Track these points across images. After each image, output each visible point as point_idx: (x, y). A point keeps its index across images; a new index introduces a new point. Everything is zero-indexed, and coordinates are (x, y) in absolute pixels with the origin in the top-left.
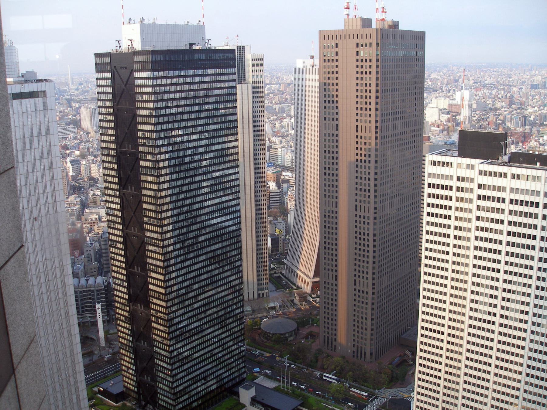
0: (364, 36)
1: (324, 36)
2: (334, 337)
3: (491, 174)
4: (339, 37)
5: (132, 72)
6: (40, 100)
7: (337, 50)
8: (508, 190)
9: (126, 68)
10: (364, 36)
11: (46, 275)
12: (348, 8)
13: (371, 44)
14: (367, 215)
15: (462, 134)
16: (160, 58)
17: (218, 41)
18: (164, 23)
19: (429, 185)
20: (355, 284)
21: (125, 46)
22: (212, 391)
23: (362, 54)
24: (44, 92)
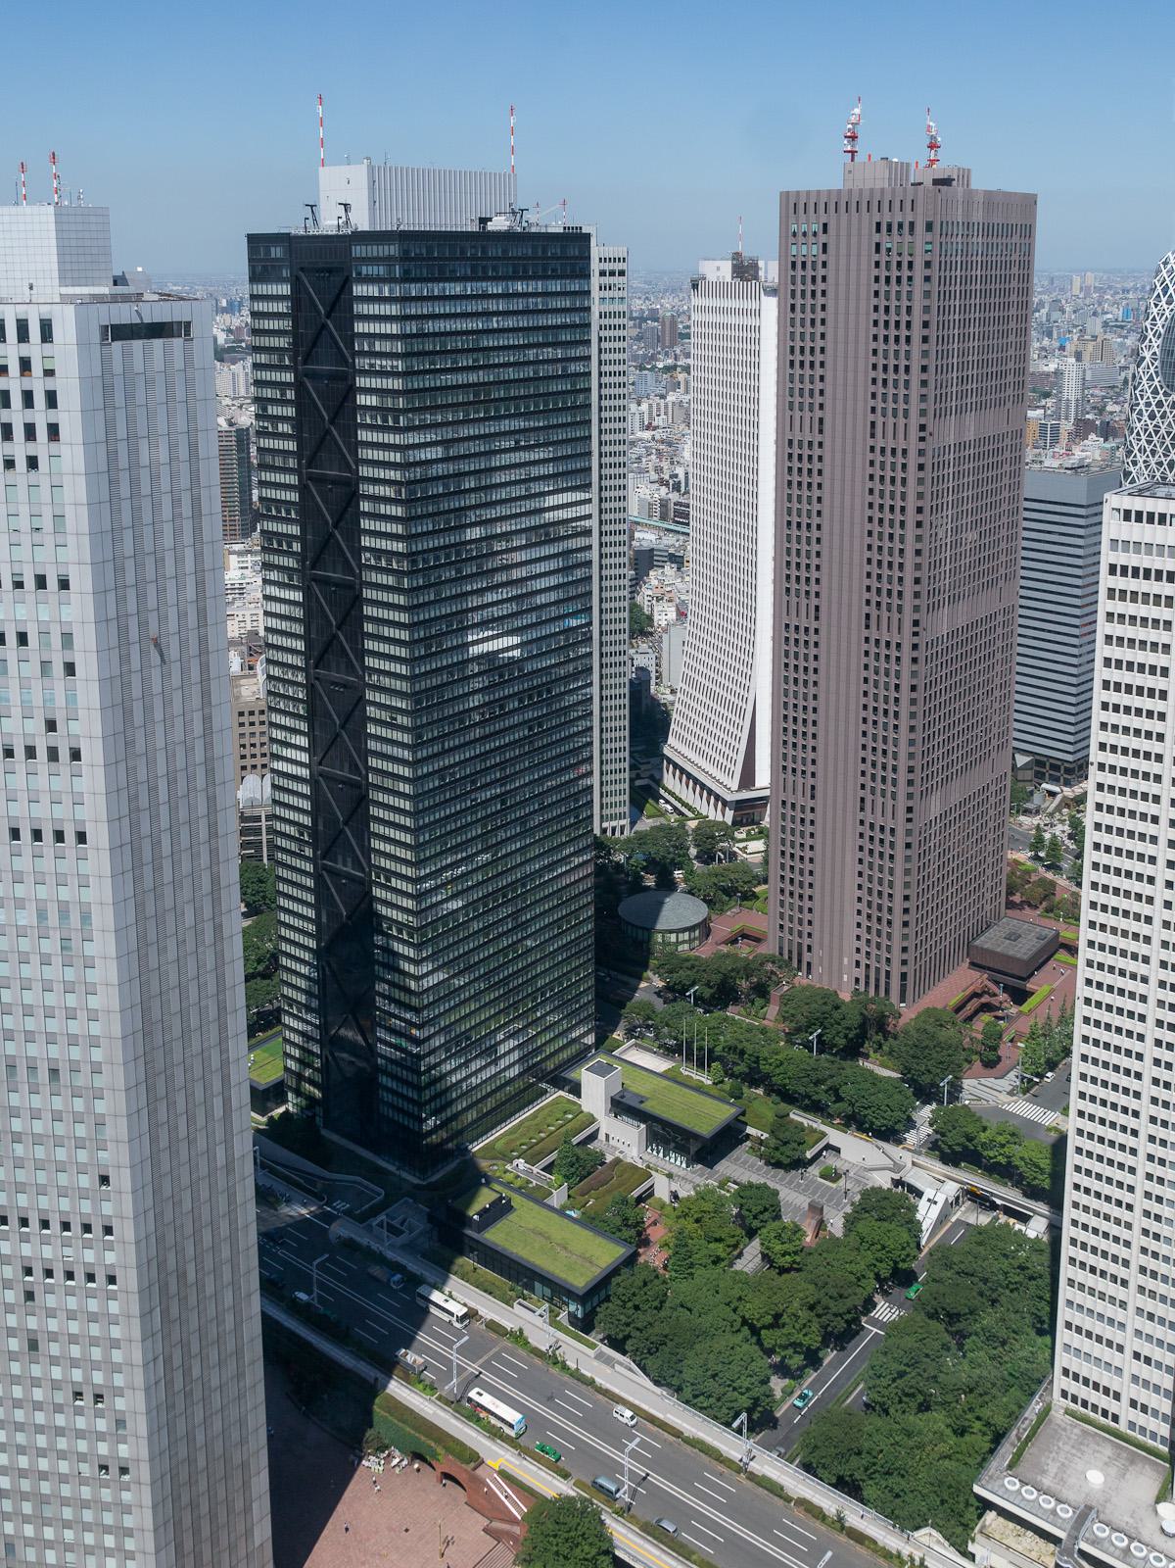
1: (793, 205)
2: (806, 941)
5: (346, 285)
6: (177, 342)
11: (171, 782)
13: (912, 224)
17: (549, 220)
19: (1112, 569)
20: (862, 809)
21: (329, 223)
22: (511, 1081)
24: (188, 324)
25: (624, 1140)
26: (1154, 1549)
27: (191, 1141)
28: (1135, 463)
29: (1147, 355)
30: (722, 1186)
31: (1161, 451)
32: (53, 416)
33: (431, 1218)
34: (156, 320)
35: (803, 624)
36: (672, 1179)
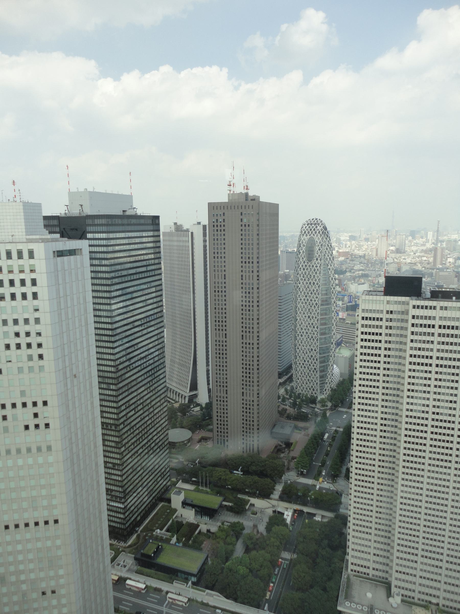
1: (212, 207)
4: (226, 208)
6: (78, 257)
8: (437, 318)
9: (77, 230)
10: (247, 207)
12: (230, 185)
14: (251, 342)
17: (143, 208)
18: (103, 191)
23: (245, 220)
24: (81, 249)
25: (189, 515)
26: (358, 604)
29: (301, 251)
30: (223, 524)
31: (307, 279)
32: (34, 289)
33: (136, 559)
35: (221, 340)
36: (206, 525)
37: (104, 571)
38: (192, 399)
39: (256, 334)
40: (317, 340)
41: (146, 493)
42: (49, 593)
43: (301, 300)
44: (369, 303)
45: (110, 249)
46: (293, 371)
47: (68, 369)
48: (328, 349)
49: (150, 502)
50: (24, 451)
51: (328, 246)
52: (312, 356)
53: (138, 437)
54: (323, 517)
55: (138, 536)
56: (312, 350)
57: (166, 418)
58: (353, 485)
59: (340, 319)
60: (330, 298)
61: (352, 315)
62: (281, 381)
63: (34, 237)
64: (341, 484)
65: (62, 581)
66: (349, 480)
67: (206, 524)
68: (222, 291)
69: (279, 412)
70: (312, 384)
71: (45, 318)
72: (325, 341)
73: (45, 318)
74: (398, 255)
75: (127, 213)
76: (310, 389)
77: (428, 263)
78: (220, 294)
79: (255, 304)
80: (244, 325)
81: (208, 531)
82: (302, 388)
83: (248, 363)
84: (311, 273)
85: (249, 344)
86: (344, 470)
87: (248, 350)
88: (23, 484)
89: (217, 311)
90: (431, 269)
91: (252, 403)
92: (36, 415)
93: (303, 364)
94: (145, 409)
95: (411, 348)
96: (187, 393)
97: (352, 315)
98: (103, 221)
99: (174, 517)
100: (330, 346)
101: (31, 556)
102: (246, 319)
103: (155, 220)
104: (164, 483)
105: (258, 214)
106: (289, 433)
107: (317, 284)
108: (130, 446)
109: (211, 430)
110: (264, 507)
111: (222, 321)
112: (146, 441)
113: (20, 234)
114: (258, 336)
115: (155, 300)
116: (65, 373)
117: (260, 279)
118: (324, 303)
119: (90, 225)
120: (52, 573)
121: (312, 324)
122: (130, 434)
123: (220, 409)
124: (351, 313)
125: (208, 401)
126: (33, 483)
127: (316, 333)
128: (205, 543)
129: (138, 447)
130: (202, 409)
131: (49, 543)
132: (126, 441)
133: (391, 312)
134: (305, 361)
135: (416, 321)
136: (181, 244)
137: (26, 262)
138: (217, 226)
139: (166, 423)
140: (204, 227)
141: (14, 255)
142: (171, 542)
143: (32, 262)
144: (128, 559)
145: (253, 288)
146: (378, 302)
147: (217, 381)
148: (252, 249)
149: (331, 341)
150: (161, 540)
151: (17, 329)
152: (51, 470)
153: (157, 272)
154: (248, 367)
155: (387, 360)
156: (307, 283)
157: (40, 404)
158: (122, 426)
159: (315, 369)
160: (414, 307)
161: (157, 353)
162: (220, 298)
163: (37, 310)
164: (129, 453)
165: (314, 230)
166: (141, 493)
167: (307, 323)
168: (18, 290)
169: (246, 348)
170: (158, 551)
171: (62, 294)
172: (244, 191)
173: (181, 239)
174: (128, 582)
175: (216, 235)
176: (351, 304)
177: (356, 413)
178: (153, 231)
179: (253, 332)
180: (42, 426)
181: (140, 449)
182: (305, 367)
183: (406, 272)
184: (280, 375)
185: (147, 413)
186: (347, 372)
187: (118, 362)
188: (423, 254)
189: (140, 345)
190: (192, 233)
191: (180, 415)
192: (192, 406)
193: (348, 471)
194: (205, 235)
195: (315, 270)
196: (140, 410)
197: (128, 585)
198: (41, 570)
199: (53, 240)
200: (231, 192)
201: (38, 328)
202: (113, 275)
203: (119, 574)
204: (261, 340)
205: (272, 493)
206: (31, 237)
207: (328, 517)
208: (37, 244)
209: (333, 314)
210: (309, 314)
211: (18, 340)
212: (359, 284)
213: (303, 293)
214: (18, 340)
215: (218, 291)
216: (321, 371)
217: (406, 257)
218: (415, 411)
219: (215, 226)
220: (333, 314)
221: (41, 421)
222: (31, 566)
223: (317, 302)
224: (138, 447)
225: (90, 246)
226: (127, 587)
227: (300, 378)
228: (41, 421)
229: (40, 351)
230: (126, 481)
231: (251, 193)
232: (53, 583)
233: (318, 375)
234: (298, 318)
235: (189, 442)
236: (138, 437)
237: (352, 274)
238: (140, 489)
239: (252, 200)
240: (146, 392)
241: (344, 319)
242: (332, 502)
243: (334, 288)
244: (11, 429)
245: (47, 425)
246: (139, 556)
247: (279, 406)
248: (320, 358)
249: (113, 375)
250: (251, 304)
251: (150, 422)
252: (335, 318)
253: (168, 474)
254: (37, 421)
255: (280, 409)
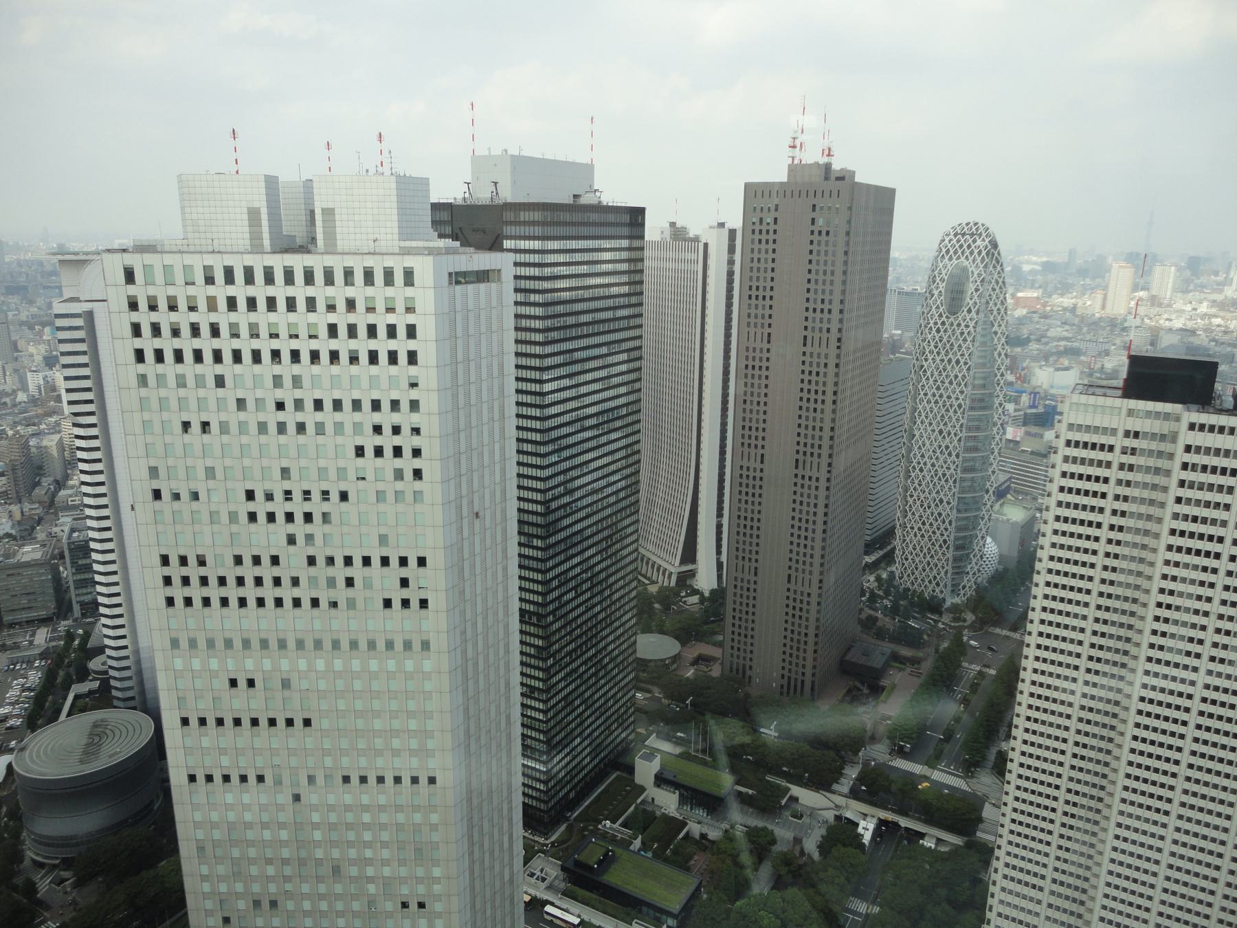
0: (827, 194)
1: (752, 191)
2: (748, 663)
3: (1212, 429)
6: (494, 285)
7: (776, 215)
10: (827, 194)
12: (794, 147)
14: (815, 475)
15: (1135, 361)
16: (445, 216)
17: (614, 192)
18: (537, 154)
23: (820, 222)
25: (668, 802)
27: (492, 868)
28: (926, 360)
29: (936, 293)
31: (943, 352)
32: (412, 345)
33: (563, 869)
34: (482, 268)
36: (698, 825)
37: (511, 881)
38: (685, 579)
39: (825, 460)
40: (955, 482)
41: (588, 750)
42: (413, 906)
43: (926, 394)
44: (1095, 412)
45: (547, 271)
46: (897, 542)
47: (465, 501)
48: (977, 502)
49: (595, 767)
50: (381, 645)
51: (997, 283)
52: (940, 514)
53: (579, 641)
54: (939, 841)
55: (570, 829)
56: (941, 501)
57: (635, 611)
58: (1013, 786)
59: (1010, 441)
60: (991, 395)
61: (1035, 435)
62: (869, 559)
63: (414, 244)
64: (984, 782)
65: (437, 888)
66: (1003, 776)
67: (699, 823)
68: (760, 368)
69: (860, 621)
70: (935, 571)
71: (430, 400)
72: (971, 486)
73: (430, 400)
74: (1156, 310)
75: (583, 201)
76: (930, 582)
77: (1226, 333)
78: (757, 372)
79: (829, 397)
80: (802, 440)
81: (703, 836)
82: (912, 578)
83: (804, 517)
84: (953, 340)
85: (810, 478)
86: (992, 756)
87: (806, 491)
88: (376, 705)
89: (748, 407)
90: (1230, 345)
91: (806, 599)
92: (404, 583)
93: (920, 529)
94: (595, 590)
95: (1176, 516)
96: (674, 566)
97: (1035, 435)
98: (537, 216)
99: (639, 801)
100: (982, 497)
101: (385, 836)
102: (807, 427)
103: (636, 216)
104: (624, 735)
105: (850, 208)
106: (879, 666)
107: (966, 363)
108: (563, 658)
109: (720, 645)
110: (817, 806)
111: (757, 429)
112: (593, 651)
113: (389, 237)
114: (830, 465)
115: (625, 378)
116: (459, 508)
117: (843, 347)
118: (976, 405)
119: (511, 223)
120: (420, 872)
121: (947, 447)
122: (565, 636)
123: (741, 604)
124: (1034, 429)
125: (716, 587)
126: (394, 705)
127: (953, 467)
128: (696, 858)
129: (579, 662)
130: (703, 599)
131: (418, 818)
132: (556, 647)
133: (1136, 435)
134: (924, 523)
135: (1192, 458)
136: (682, 266)
137: (398, 292)
138: (761, 232)
139: (634, 621)
140: (732, 233)
141: (379, 278)
142: (632, 848)
143: (409, 291)
144: (552, 869)
145: (826, 365)
146: (1108, 411)
147: (737, 549)
148: (832, 283)
149: (984, 485)
150: (613, 840)
151: (377, 418)
152: (428, 686)
153: (633, 322)
154: (803, 525)
155: (1115, 535)
156: (942, 360)
157: (413, 562)
158: (551, 618)
159: (945, 541)
160: (1192, 427)
161: (623, 483)
162: (756, 381)
163: (414, 385)
164: (560, 671)
165: (969, 246)
166: (579, 749)
167: (936, 445)
168: (363, 345)
169: (802, 486)
170: (607, 861)
171: (460, 357)
172: (823, 160)
173: (682, 256)
174: (548, 908)
175: (756, 251)
176: (1034, 411)
177: (1033, 640)
178: (630, 237)
179: (819, 456)
180: (415, 604)
181: (581, 665)
182: (923, 536)
183: (1169, 347)
184: (869, 548)
185: (598, 599)
186: (1015, 554)
187: (549, 495)
188: (1214, 310)
189: (593, 465)
190: (706, 245)
191: (659, 610)
192: (683, 594)
193: (1002, 759)
194: (732, 250)
195: (962, 333)
196: (586, 591)
197: (548, 913)
198: (402, 862)
199: (449, 251)
200: (796, 162)
201: (416, 419)
202: (549, 323)
203: (533, 892)
204: (834, 472)
205: (836, 781)
206: (408, 244)
207: (953, 844)
208: (420, 258)
209: (995, 430)
210: (941, 426)
211: (378, 440)
212: (1057, 370)
213: (931, 381)
214: (378, 440)
215: (753, 367)
216: (957, 548)
217: (1173, 317)
218: (1170, 650)
219: (757, 232)
220: (995, 430)
221: (414, 596)
222: (386, 854)
223: (960, 401)
224: (579, 662)
225: (516, 264)
226: (546, 917)
227: (910, 558)
228: (414, 596)
229: (417, 463)
230: (552, 723)
231: (836, 166)
232: (421, 889)
233: (950, 555)
234: (916, 432)
235: (673, 662)
236: (579, 641)
237: (1041, 347)
238: (578, 740)
239: (838, 179)
240: (598, 558)
241: (1017, 443)
242: (963, 816)
243: (1002, 375)
244: (360, 604)
245: (424, 603)
246: (570, 864)
247: (861, 610)
248: (958, 519)
249: (540, 520)
250: (820, 397)
251: (603, 615)
252: (998, 437)
253: (632, 719)
254: (405, 594)
255: (863, 616)
